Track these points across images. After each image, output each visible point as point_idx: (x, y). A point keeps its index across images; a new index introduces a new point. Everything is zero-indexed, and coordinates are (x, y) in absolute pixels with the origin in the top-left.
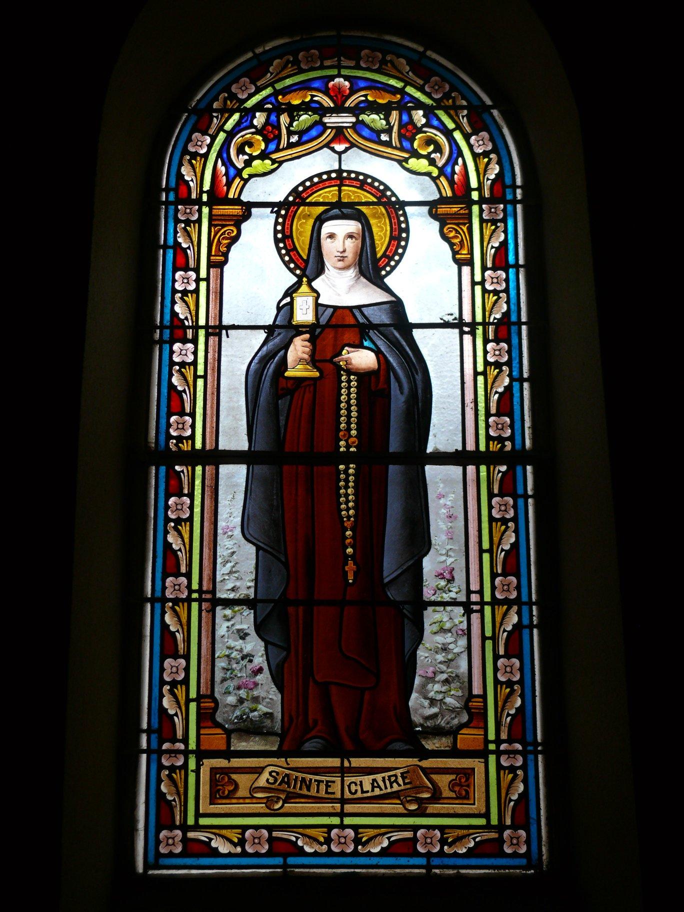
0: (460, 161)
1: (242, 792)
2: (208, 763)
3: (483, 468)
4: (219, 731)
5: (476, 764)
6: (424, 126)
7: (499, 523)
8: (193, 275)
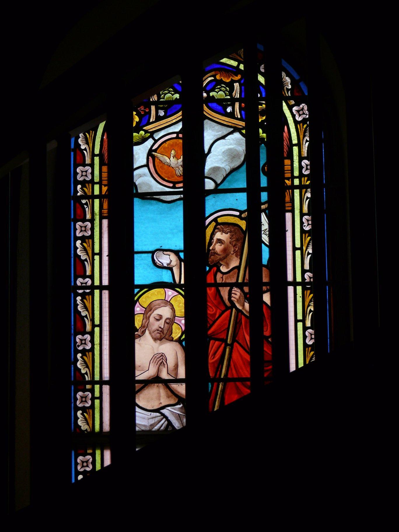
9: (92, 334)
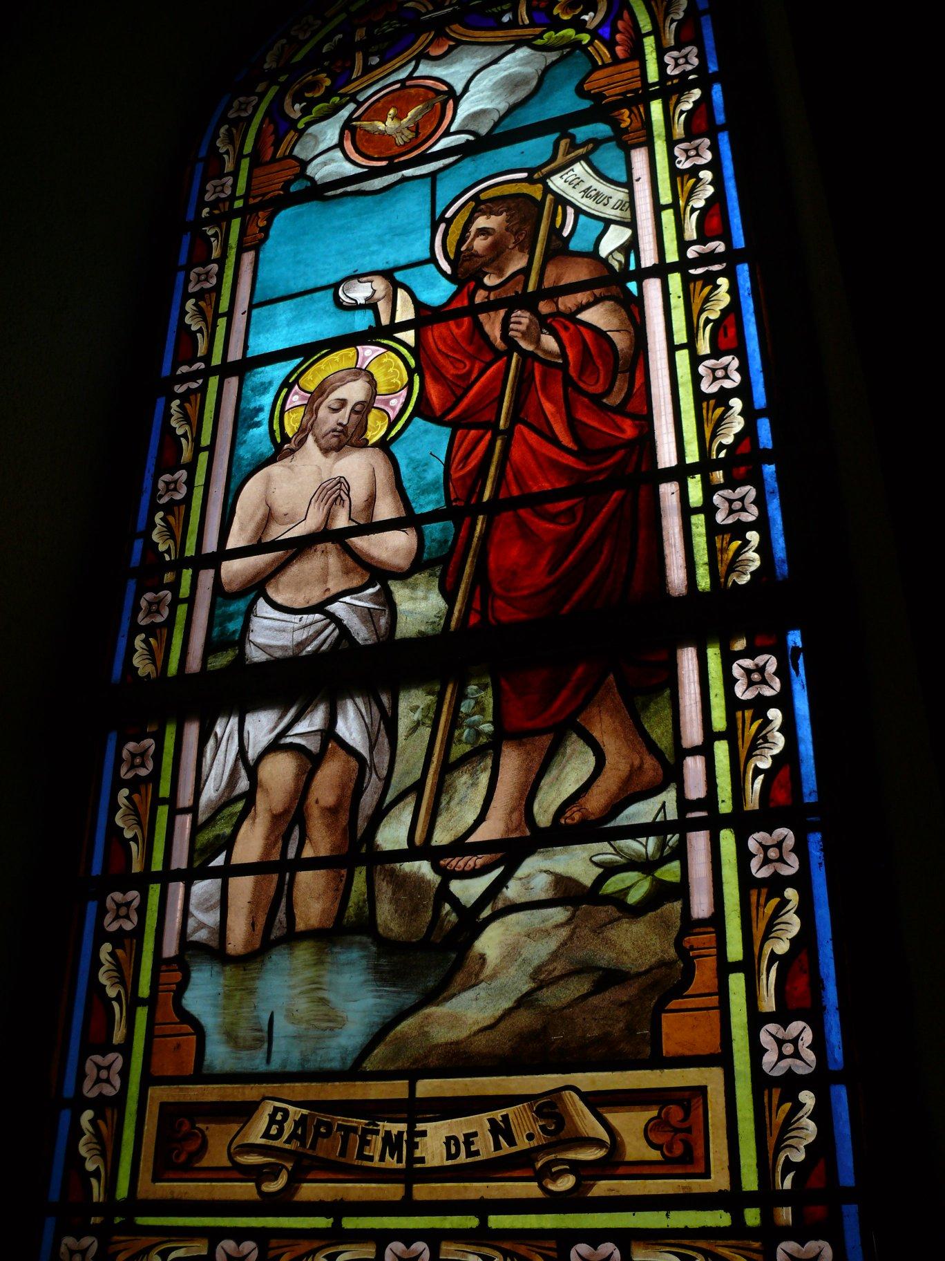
0: (626, 15)
1: (217, 1156)
2: (159, 1094)
3: (713, 654)
4: (187, 1028)
5: (712, 1078)
6: (573, 137)
7: (712, 402)
8: (168, 595)
9: (191, 468)
